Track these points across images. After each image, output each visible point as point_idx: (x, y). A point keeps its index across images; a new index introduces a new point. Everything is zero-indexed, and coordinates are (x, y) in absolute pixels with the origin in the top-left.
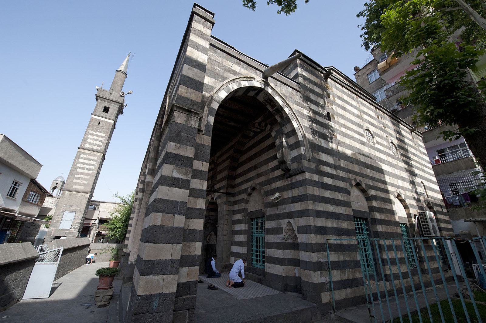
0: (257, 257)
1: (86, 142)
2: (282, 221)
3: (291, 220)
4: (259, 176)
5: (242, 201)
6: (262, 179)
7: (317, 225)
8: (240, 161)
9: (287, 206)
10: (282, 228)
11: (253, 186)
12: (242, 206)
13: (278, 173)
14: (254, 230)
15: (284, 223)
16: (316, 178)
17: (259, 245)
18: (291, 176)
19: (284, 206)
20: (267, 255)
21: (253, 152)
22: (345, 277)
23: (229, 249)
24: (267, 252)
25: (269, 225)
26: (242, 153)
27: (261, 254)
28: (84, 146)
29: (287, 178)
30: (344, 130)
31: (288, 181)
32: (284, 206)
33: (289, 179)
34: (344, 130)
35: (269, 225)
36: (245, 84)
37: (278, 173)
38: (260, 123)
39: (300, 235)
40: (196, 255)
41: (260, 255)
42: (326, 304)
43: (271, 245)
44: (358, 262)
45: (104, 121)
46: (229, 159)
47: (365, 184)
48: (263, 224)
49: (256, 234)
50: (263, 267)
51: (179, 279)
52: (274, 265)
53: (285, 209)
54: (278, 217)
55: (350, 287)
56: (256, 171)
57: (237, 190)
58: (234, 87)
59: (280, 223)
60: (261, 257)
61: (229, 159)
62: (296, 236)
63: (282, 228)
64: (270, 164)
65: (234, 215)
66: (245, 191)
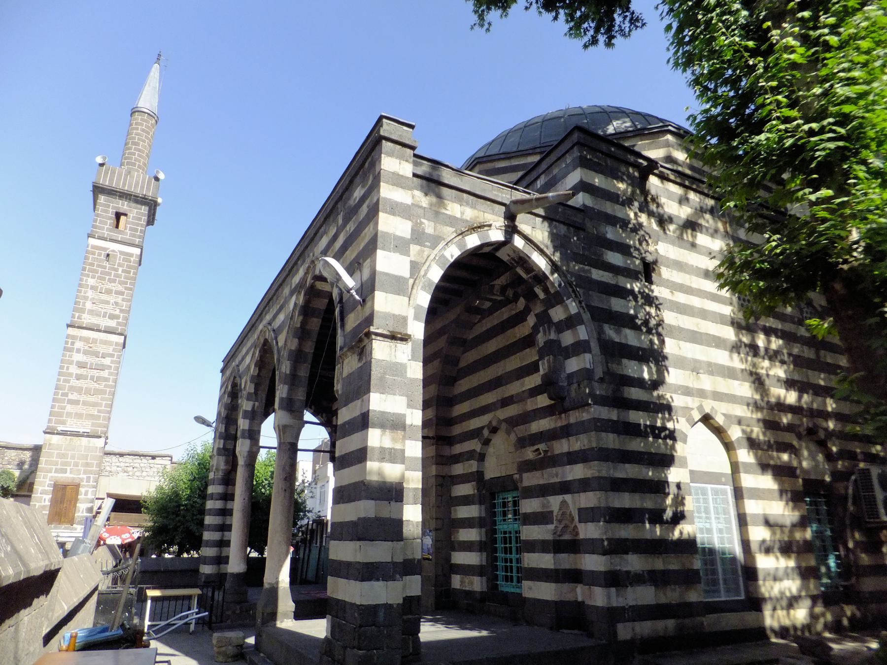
0: (506, 571)
1: (82, 311)
2: (551, 499)
3: (568, 497)
4: (506, 402)
5: (470, 455)
6: (512, 411)
7: (612, 506)
8: (463, 364)
9: (559, 470)
10: (552, 512)
11: (494, 424)
12: (471, 466)
13: (543, 401)
14: (499, 518)
15: (554, 502)
16: (613, 414)
17: (511, 548)
18: (565, 411)
19: (554, 469)
20: (526, 566)
21: (491, 346)
22: (663, 600)
23: (448, 558)
24: (526, 559)
25: (529, 506)
26: (467, 345)
27: (514, 564)
28: (79, 318)
29: (560, 413)
30: (681, 298)
31: (561, 418)
32: (554, 470)
33: (563, 415)
34: (681, 298)
35: (529, 506)
36: (473, 241)
37: (543, 401)
38: (503, 289)
39: (583, 524)
40: (414, 559)
41: (511, 567)
42: (626, 642)
43: (532, 546)
44: (697, 572)
45: (122, 253)
46: (439, 360)
47: (724, 415)
48: (516, 503)
49: (501, 527)
50: (518, 591)
51: (404, 588)
52: (539, 583)
53: (557, 475)
54: (544, 491)
55: (673, 617)
56: (499, 390)
57: (457, 430)
58: (453, 253)
59: (548, 502)
60: (515, 570)
61: (439, 360)
62: (576, 526)
63: (552, 512)
64: (527, 379)
65: (455, 486)
66: (476, 434)
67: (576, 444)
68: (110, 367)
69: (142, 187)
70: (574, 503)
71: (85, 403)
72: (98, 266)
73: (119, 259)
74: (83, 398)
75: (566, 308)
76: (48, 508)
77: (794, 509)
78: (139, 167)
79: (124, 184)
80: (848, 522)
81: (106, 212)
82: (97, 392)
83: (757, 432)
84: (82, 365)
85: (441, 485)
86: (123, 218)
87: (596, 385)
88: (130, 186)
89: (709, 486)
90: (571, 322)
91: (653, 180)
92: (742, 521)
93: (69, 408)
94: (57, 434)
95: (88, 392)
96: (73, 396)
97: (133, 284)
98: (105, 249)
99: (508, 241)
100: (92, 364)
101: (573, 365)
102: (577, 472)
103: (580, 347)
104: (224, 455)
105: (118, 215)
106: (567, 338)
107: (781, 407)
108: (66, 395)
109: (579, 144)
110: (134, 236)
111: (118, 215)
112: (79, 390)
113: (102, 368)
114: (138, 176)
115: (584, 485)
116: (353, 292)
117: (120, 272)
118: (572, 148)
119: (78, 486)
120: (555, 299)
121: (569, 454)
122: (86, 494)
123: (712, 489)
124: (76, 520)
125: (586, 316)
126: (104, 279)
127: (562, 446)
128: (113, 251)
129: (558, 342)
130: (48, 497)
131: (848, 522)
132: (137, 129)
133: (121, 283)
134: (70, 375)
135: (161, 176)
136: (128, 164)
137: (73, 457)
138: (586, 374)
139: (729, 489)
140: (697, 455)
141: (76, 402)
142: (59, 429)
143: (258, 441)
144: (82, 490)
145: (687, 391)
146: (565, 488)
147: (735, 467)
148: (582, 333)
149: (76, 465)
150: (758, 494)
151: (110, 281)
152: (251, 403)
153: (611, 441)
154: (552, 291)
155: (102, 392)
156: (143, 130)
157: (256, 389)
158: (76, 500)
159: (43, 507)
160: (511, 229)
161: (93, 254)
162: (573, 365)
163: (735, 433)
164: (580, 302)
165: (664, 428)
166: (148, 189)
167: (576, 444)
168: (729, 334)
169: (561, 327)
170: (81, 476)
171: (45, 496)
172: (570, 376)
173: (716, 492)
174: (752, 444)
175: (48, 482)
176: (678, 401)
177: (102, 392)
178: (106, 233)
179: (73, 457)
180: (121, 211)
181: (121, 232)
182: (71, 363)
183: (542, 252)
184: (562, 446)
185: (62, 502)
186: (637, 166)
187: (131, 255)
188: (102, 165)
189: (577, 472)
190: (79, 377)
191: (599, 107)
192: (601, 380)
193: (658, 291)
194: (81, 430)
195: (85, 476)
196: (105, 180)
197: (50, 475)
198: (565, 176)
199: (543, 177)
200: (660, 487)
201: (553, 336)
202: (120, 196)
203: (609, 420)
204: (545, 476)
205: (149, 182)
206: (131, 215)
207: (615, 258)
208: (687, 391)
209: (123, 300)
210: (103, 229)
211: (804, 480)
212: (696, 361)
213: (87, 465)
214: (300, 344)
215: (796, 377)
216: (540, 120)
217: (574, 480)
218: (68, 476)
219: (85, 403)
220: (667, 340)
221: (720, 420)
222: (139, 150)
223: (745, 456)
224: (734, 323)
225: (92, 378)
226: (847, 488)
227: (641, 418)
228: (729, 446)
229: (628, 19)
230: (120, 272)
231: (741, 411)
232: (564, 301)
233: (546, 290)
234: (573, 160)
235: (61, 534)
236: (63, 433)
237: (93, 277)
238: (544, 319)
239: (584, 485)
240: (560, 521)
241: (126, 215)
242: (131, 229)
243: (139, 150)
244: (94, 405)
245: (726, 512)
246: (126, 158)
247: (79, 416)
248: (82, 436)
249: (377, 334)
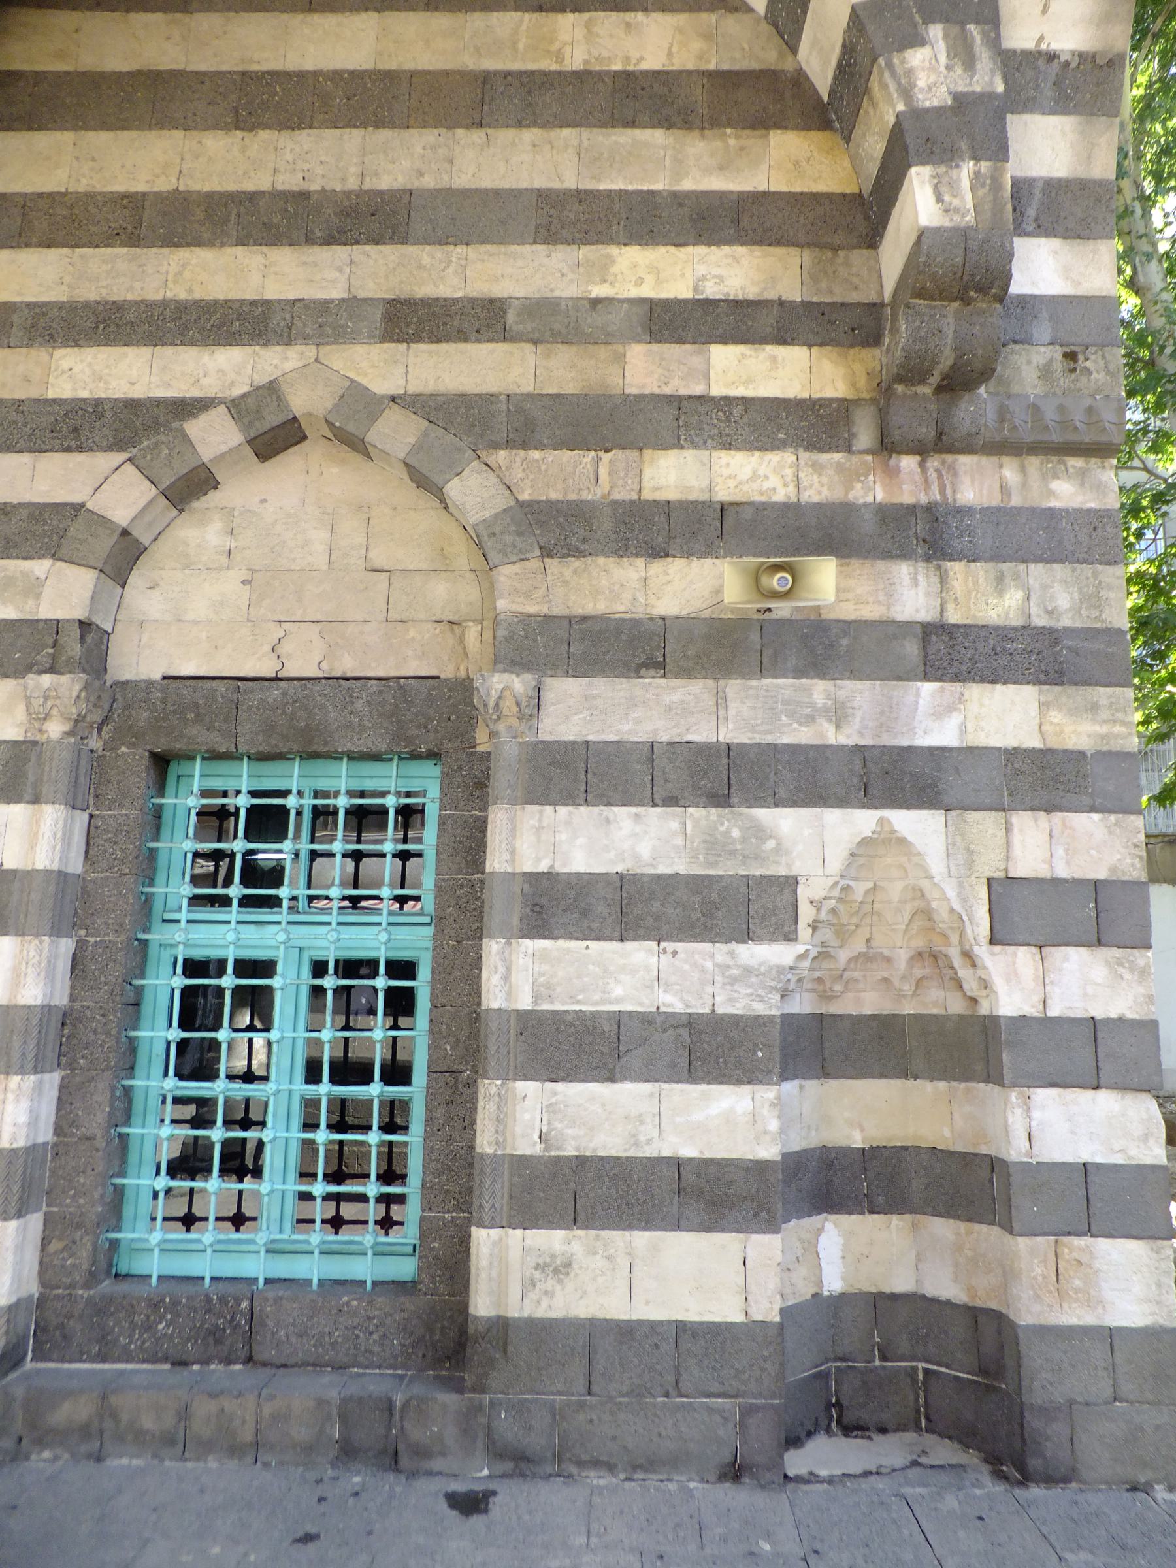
2: (786, 822)
3: (920, 827)
32: (819, 690)
59: (759, 832)
70: (963, 853)
102: (1005, 716)
146: (895, 777)
204: (735, 707)
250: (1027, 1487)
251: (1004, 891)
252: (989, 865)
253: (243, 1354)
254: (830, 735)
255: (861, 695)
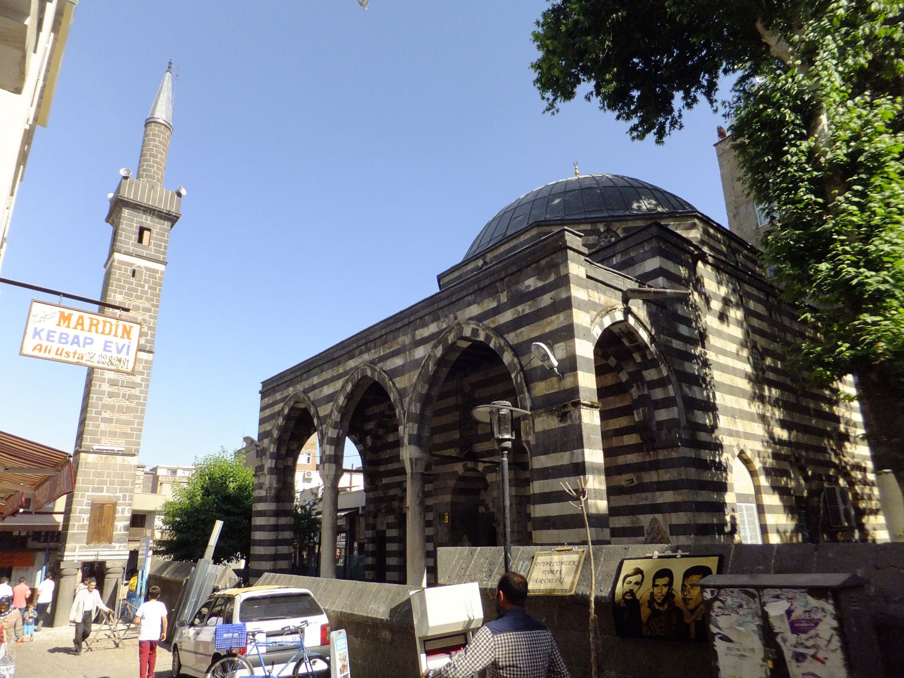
2: (641, 517)
3: (659, 517)
30: (722, 359)
32: (644, 495)
33: (652, 453)
34: (722, 359)
36: (607, 322)
45: (147, 269)
59: (638, 519)
67: (666, 476)
68: (140, 385)
69: (166, 203)
70: (665, 520)
71: (118, 421)
72: (125, 282)
73: (145, 276)
74: (116, 416)
75: (660, 371)
76: (87, 528)
77: (793, 518)
78: (158, 180)
79: (148, 199)
80: (819, 528)
81: (131, 226)
82: (129, 410)
83: (770, 461)
84: (113, 383)
85: (520, 504)
86: (146, 233)
87: (682, 431)
88: (154, 201)
89: (743, 505)
90: (662, 383)
91: (700, 264)
92: (764, 529)
93: (103, 427)
94: (93, 453)
95: (120, 410)
96: (106, 415)
97: (158, 301)
98: (131, 265)
99: (626, 320)
100: (123, 382)
101: (662, 415)
102: (668, 497)
103: (668, 403)
104: (276, 474)
105: (142, 230)
106: (658, 394)
107: (781, 442)
108: (100, 413)
109: (658, 238)
110: (158, 252)
111: (142, 230)
112: (111, 408)
113: (133, 386)
114: (161, 191)
115: (675, 507)
116: (556, 369)
117: (146, 288)
118: (651, 239)
119: (115, 505)
120: (653, 364)
121: (658, 482)
122: (123, 512)
123: (746, 507)
124: (115, 538)
125: (673, 378)
126: (131, 295)
127: (652, 477)
128: (139, 267)
129: (649, 396)
130: (86, 516)
131: (819, 528)
132: (155, 141)
133: (148, 300)
134: (103, 393)
135: (183, 192)
136: (147, 176)
137: (109, 476)
138: (672, 424)
139: (754, 506)
140: (739, 481)
141: (109, 421)
142: (95, 447)
143: (341, 465)
144: (119, 508)
145: (731, 433)
146: (655, 509)
147: (758, 489)
148: (671, 391)
149: (112, 483)
150: (773, 509)
151: (138, 297)
152: (337, 431)
153: (692, 473)
154: (649, 357)
155: (134, 410)
156: (160, 142)
157: (342, 419)
158: (114, 519)
159: (82, 527)
160: (627, 311)
161: (120, 269)
162: (662, 415)
163: (757, 465)
164: (669, 367)
165: (714, 461)
166: (171, 204)
167: (666, 476)
168: (745, 385)
169: (653, 385)
170: (117, 494)
171: (83, 516)
172: (660, 423)
173: (747, 509)
174: (768, 472)
175: (86, 501)
176: (726, 441)
177: (134, 410)
178: (131, 248)
179: (109, 476)
180: (145, 226)
181: (145, 248)
182: (103, 380)
183: (645, 328)
184: (652, 477)
185: (100, 521)
186: (691, 253)
187: (156, 271)
188: (126, 178)
189: (668, 497)
190: (111, 395)
191: (622, 178)
192: (685, 428)
193: (711, 356)
194: (116, 449)
195: (121, 495)
196: (129, 194)
197: (87, 494)
198: (644, 259)
199: (619, 256)
200: (720, 507)
201: (646, 392)
202: (144, 211)
203: (691, 458)
204: (634, 499)
205: (172, 198)
206: (154, 230)
207: (683, 330)
208: (731, 433)
209: (150, 317)
210: (128, 244)
211: (796, 497)
212: (733, 409)
213: (123, 483)
214: (429, 389)
215: (787, 419)
216: (577, 187)
217: (665, 503)
218: (105, 495)
219: (118, 421)
220: (717, 393)
221: (749, 454)
222: (158, 163)
223: (763, 481)
224: (748, 377)
225: (124, 396)
226: (819, 502)
227: (707, 455)
228: (753, 474)
229: (669, 121)
230: (146, 288)
231: (758, 446)
232: (659, 366)
233: (644, 356)
234: (652, 248)
235: (100, 553)
236: (99, 452)
237: (121, 293)
238: (637, 377)
239: (675, 507)
240: (649, 534)
241: (149, 230)
242: (155, 245)
243: (158, 163)
244: (127, 423)
245: (753, 524)
246: (144, 170)
247: (113, 434)
248: (117, 454)
249: (584, 405)
250: (165, 505)
251: (672, 527)
252: (669, 523)
253: (154, 129)
254: (646, 503)
255: (649, 495)
